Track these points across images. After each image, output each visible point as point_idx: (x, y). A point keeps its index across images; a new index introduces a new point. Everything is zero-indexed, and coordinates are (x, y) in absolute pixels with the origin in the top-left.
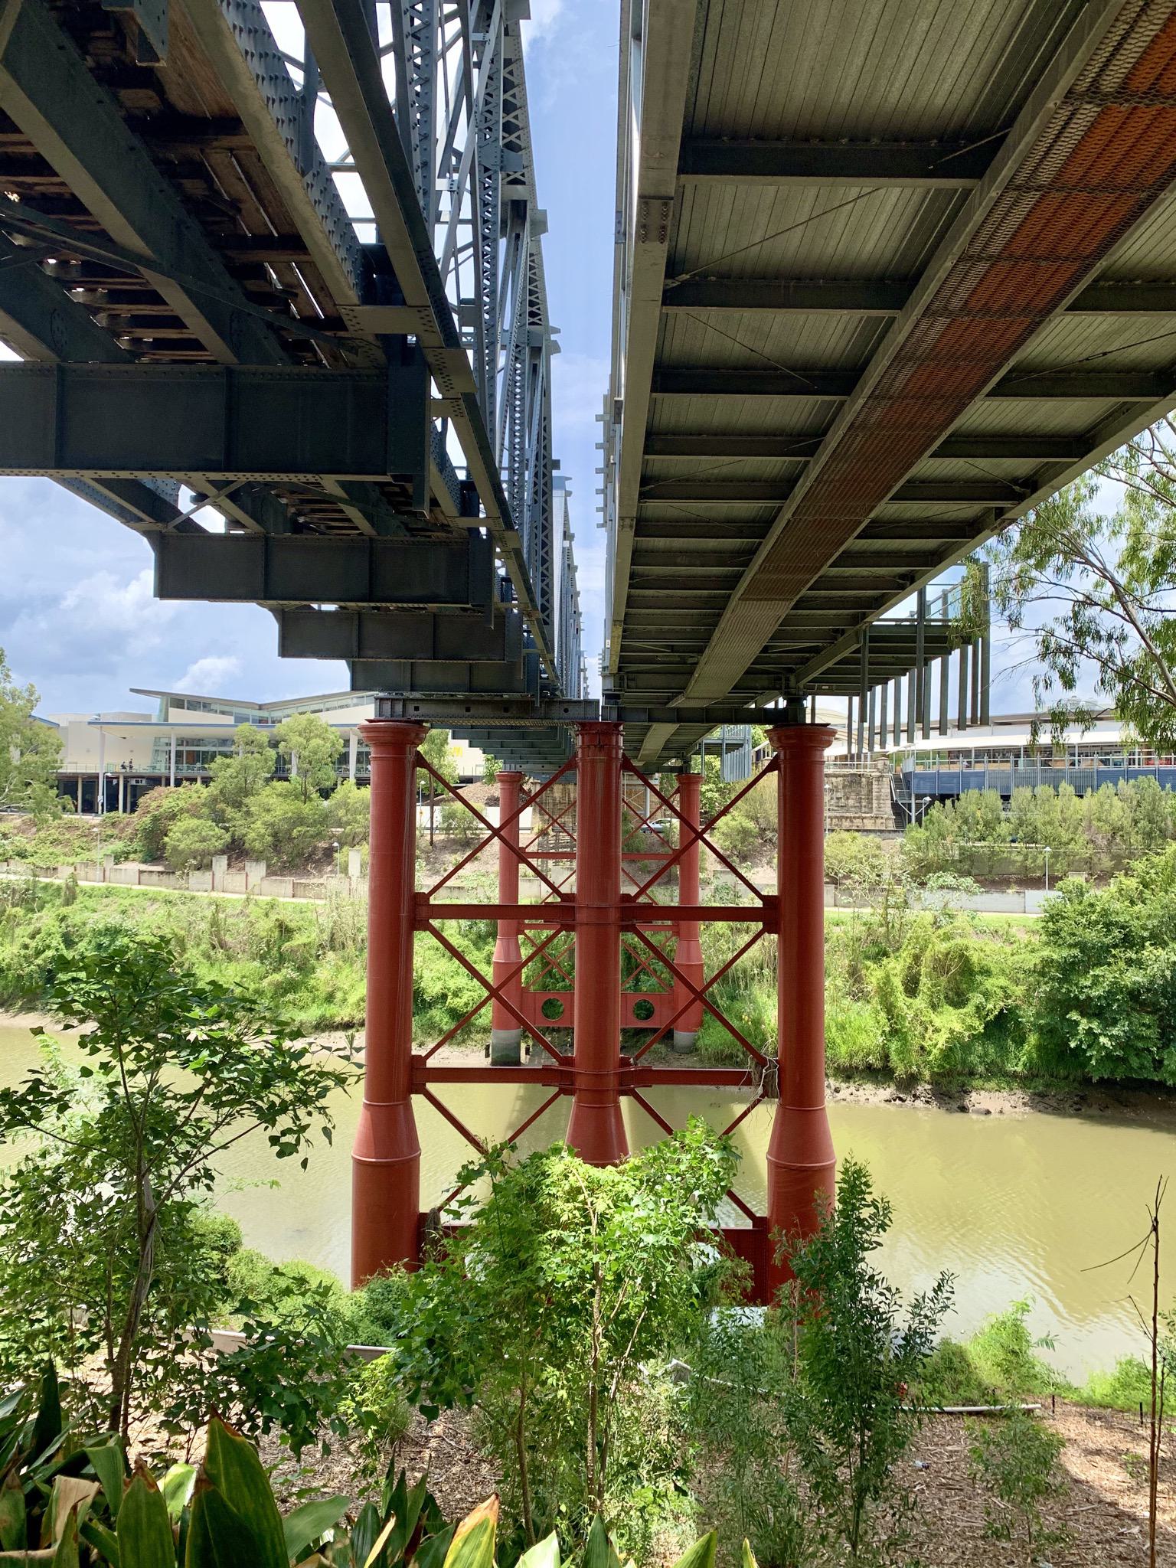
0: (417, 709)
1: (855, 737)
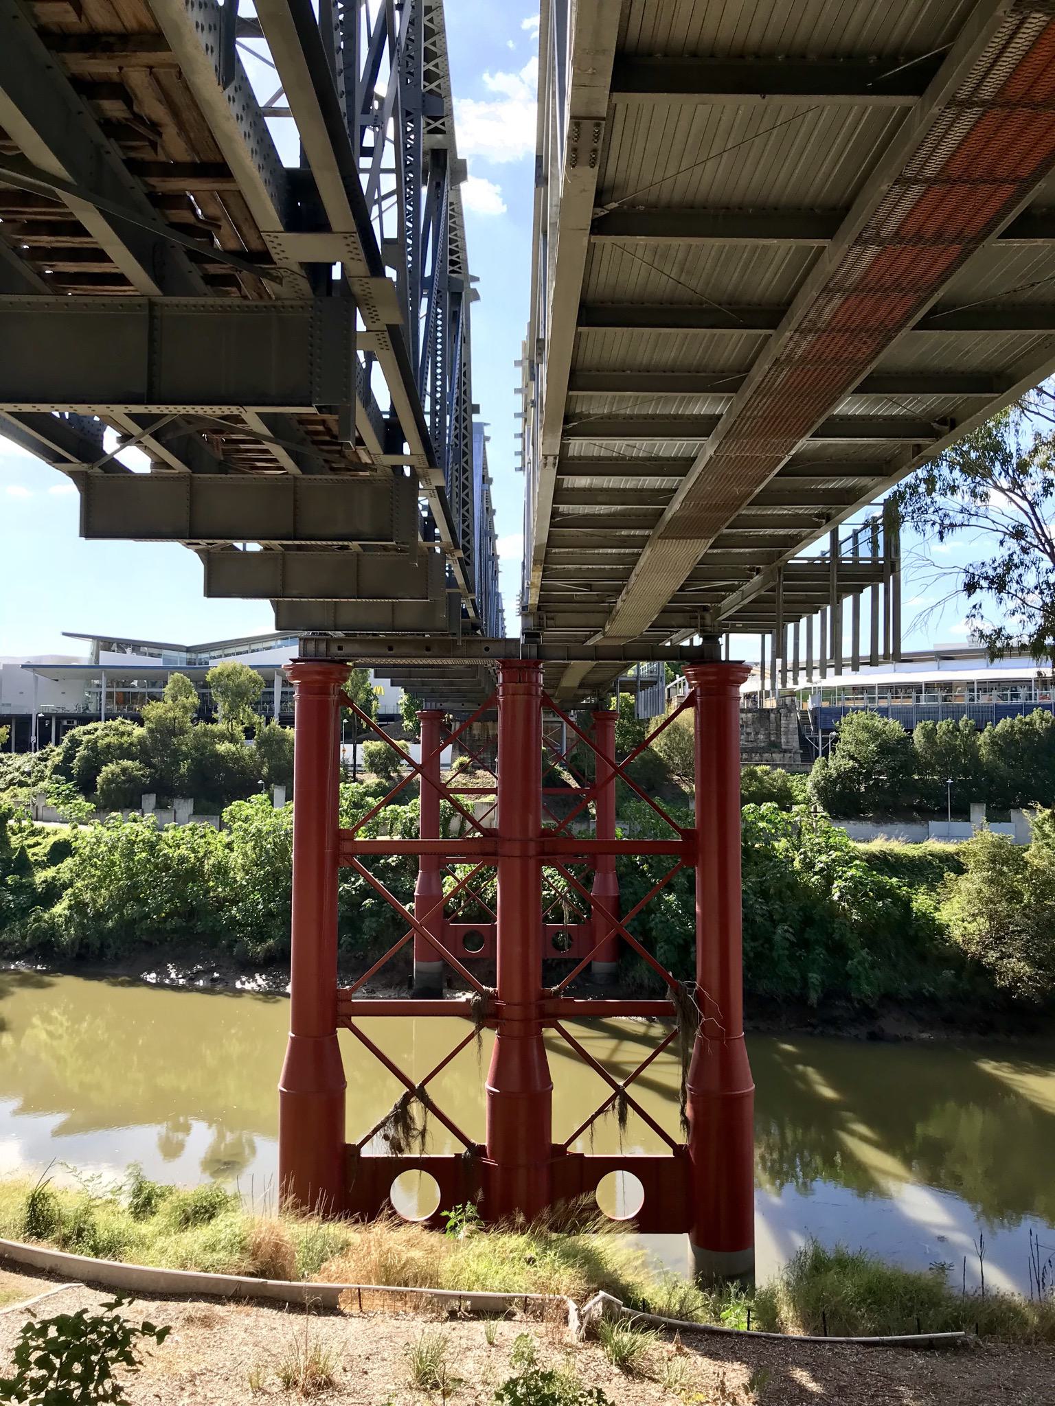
0: (340, 648)
1: (768, 671)
